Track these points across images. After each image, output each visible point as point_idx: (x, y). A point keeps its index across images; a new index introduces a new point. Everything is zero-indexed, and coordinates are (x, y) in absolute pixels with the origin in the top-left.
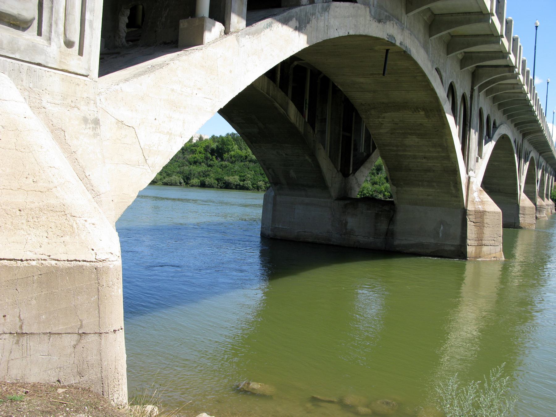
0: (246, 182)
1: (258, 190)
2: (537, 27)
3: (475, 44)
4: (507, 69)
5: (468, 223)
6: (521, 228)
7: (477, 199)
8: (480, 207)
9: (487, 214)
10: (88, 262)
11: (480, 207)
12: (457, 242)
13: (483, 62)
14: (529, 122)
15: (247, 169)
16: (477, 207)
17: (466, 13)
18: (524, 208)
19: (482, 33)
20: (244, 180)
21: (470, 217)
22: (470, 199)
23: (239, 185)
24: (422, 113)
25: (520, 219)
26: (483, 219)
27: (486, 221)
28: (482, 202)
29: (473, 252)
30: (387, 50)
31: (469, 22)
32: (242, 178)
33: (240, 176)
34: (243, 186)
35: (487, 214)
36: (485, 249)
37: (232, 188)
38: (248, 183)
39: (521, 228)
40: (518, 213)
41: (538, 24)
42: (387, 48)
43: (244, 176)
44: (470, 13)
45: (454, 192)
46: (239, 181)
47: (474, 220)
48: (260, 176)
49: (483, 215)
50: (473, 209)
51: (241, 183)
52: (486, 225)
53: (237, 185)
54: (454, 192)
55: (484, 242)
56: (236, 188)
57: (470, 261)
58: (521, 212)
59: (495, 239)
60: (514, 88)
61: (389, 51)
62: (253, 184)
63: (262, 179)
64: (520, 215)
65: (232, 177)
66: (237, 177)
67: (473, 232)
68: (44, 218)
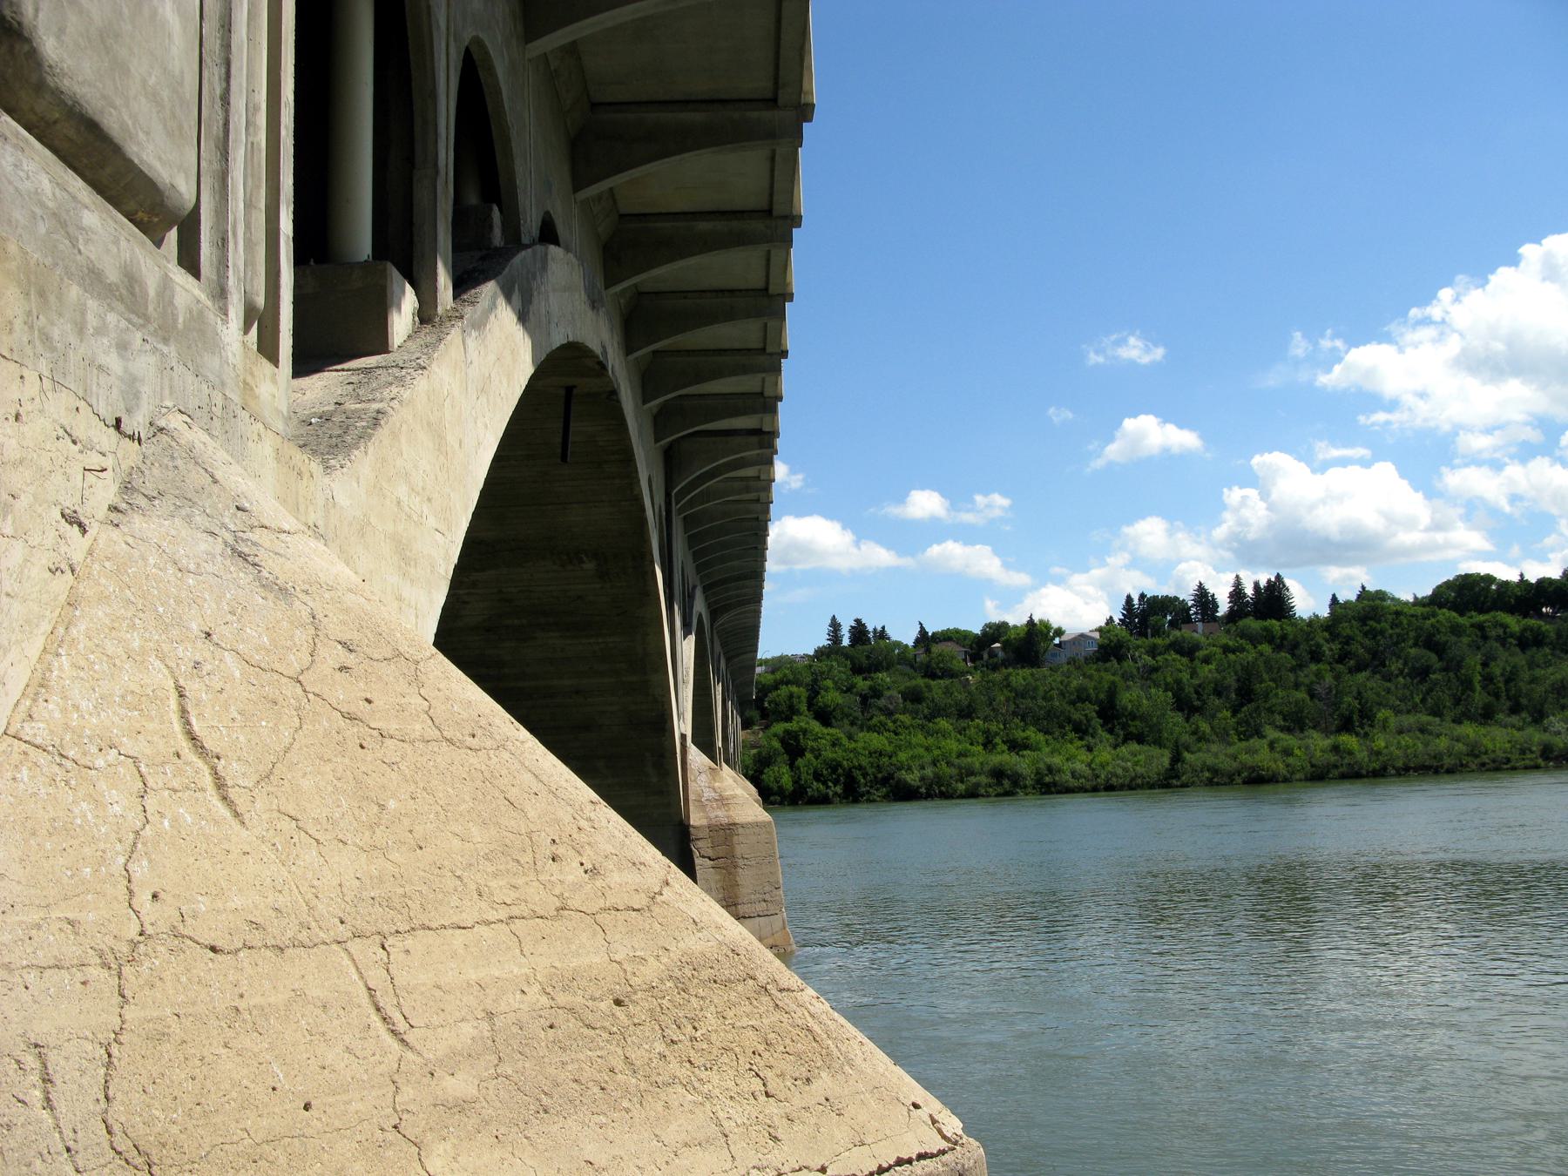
3: (717, 374)
4: (754, 439)
5: (698, 861)
7: (708, 794)
8: (719, 813)
9: (741, 830)
10: (932, 1156)
11: (721, 815)
13: (712, 420)
14: (738, 578)
16: (712, 815)
17: (722, 291)
19: (737, 345)
21: (700, 844)
22: (692, 797)
24: (590, 566)
26: (731, 846)
27: (739, 850)
28: (723, 801)
30: (569, 390)
31: (730, 315)
35: (741, 830)
42: (570, 381)
44: (731, 291)
45: (654, 780)
47: (710, 853)
49: (731, 836)
50: (704, 822)
52: (741, 862)
54: (654, 780)
59: (767, 897)
60: (748, 490)
61: (575, 391)
67: (713, 885)
68: (711, 1020)
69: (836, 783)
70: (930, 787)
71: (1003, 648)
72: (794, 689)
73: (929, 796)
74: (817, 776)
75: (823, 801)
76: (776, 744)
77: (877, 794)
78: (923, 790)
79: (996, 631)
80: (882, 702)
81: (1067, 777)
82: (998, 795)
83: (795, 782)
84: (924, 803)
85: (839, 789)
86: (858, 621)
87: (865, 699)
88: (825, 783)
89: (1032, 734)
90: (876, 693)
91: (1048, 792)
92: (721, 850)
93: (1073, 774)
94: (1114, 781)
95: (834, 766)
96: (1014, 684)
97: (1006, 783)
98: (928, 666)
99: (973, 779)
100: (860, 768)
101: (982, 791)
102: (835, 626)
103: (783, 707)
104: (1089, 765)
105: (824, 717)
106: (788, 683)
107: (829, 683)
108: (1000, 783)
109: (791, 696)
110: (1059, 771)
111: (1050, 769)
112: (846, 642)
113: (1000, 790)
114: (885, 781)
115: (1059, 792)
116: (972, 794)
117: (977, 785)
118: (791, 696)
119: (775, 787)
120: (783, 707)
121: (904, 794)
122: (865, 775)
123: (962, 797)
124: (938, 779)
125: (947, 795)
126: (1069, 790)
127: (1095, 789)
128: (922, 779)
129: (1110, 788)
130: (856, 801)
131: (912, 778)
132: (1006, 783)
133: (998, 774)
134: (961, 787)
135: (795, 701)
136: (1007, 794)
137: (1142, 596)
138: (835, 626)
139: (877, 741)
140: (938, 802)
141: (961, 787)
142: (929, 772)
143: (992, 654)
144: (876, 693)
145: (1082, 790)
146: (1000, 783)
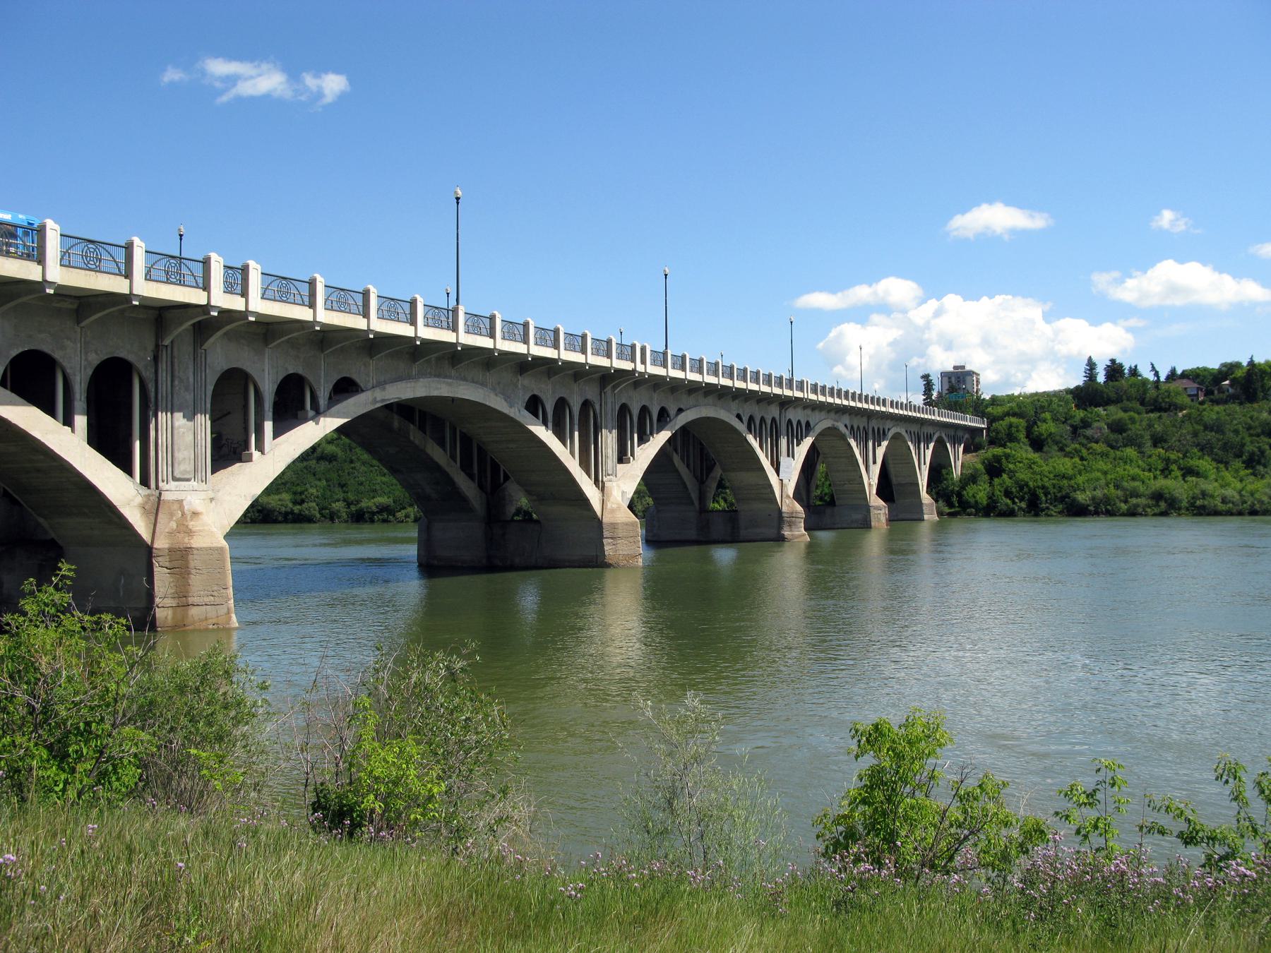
0: (305, 505)
1: (332, 519)
2: (458, 199)
6: (608, 566)
12: (142, 604)
15: (311, 478)
18: (614, 526)
20: (302, 502)
23: (292, 512)
25: (606, 548)
26: (187, 561)
27: (192, 564)
29: (170, 617)
32: (298, 498)
33: (295, 493)
34: (300, 514)
36: (194, 611)
37: (275, 521)
38: (311, 507)
39: (608, 566)
40: (601, 537)
41: (460, 193)
43: (301, 493)
46: (290, 505)
47: (167, 564)
48: (337, 490)
51: (297, 509)
52: (193, 571)
53: (287, 514)
55: (191, 600)
56: (286, 521)
57: (163, 632)
58: (606, 534)
62: (321, 509)
63: (341, 495)
64: (605, 541)
65: (277, 497)
66: (286, 497)
69: (1022, 499)
70: (1097, 505)
71: (1231, 385)
72: (1014, 420)
73: (1097, 513)
74: (1008, 494)
75: (1009, 514)
76: (980, 466)
77: (1053, 510)
78: (1091, 508)
79: (1229, 370)
80: (1089, 432)
81: (1218, 502)
82: (1155, 515)
83: (990, 498)
84: (1091, 519)
85: (1023, 505)
86: (1113, 361)
87: (1075, 430)
88: (1012, 499)
89: (1205, 464)
90: (1086, 424)
91: (1200, 514)
92: (176, 564)
93: (1224, 501)
94: (1257, 507)
95: (1022, 486)
96: (1206, 419)
97: (1163, 505)
98: (1156, 400)
99: (1134, 501)
100: (1043, 487)
101: (1140, 510)
102: (1091, 365)
103: (1003, 435)
104: (1240, 492)
105: (1037, 444)
106: (1014, 415)
107: (1047, 415)
108: (1157, 505)
109: (1011, 426)
110: (1212, 496)
111: (1204, 494)
112: (1101, 378)
113: (1156, 510)
114: (1062, 499)
115: (1209, 514)
116: (1132, 513)
117: (1137, 506)
118: (1011, 426)
119: (972, 500)
120: (1003, 435)
121: (1077, 511)
122: (1046, 494)
123: (1123, 515)
124: (1107, 500)
125: (1110, 514)
126: (1216, 513)
127: (1240, 513)
128: (1093, 498)
129: (1253, 513)
130: (1037, 515)
131: (1081, 497)
132: (1163, 505)
133: (1158, 496)
134: (1124, 507)
135: (1014, 430)
136: (1164, 514)
137: (249, 459)
138: (1091, 365)
139: (1065, 464)
140: (1102, 518)
141: (1124, 507)
142: (1099, 493)
143: (1221, 391)
144: (1086, 424)
145: (1229, 513)
146: (1157, 505)
